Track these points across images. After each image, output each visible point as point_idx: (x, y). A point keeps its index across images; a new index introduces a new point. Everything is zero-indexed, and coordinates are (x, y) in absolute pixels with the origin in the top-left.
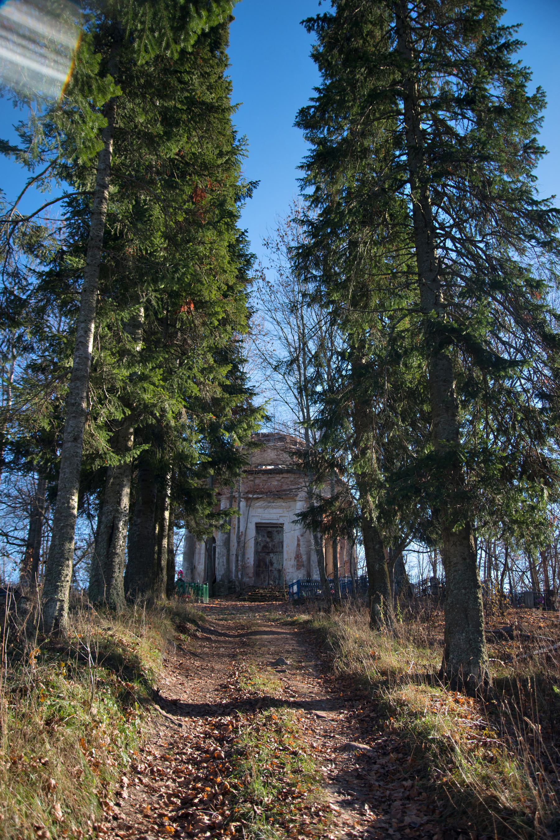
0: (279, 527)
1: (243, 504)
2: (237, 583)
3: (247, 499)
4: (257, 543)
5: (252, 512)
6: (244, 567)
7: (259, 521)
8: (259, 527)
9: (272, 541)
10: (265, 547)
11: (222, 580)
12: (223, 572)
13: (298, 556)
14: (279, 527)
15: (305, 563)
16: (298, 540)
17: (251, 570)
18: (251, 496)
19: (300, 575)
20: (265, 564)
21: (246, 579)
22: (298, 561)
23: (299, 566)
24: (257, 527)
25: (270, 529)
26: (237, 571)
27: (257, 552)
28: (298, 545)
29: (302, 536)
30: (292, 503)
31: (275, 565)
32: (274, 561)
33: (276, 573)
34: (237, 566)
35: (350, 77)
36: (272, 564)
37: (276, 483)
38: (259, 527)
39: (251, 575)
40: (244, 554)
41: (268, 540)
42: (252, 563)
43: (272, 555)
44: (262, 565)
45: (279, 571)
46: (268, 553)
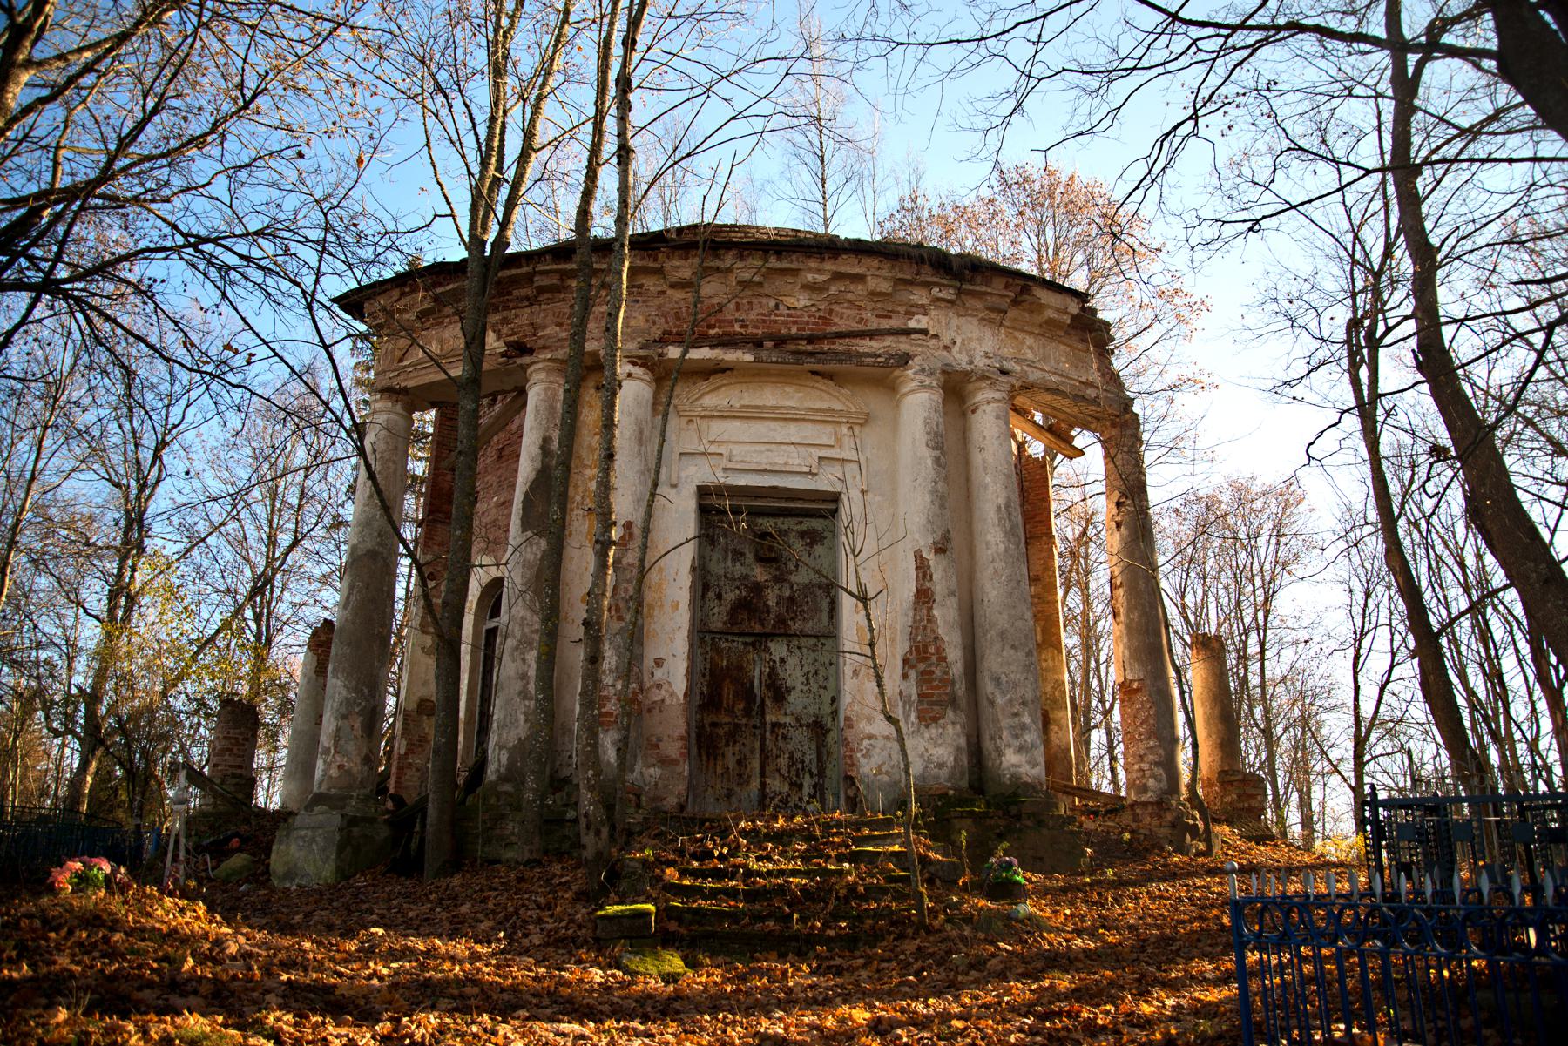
0: (818, 512)
1: (633, 392)
2: (587, 802)
3: (665, 377)
4: (703, 583)
5: (682, 437)
6: (637, 707)
7: (722, 479)
8: (713, 506)
9: (780, 579)
10: (749, 604)
11: (511, 775)
12: (521, 730)
13: (922, 655)
14: (818, 512)
15: (960, 689)
16: (922, 566)
17: (672, 725)
18: (674, 352)
19: (934, 751)
20: (747, 694)
21: (646, 773)
22: (925, 677)
23: (930, 709)
24: (704, 511)
25: (767, 524)
26: (592, 729)
27: (701, 634)
28: (924, 597)
29: (940, 549)
30: (872, 401)
31: (796, 701)
32: (793, 674)
33: (800, 740)
34: (591, 697)
35: (1402, 995)
36: (779, 693)
37: (801, 300)
38: (713, 506)
39: (673, 749)
40: (635, 639)
41: (760, 574)
42: (680, 685)
43: (778, 649)
44: (729, 697)
45: (818, 729)
46: (760, 641)
